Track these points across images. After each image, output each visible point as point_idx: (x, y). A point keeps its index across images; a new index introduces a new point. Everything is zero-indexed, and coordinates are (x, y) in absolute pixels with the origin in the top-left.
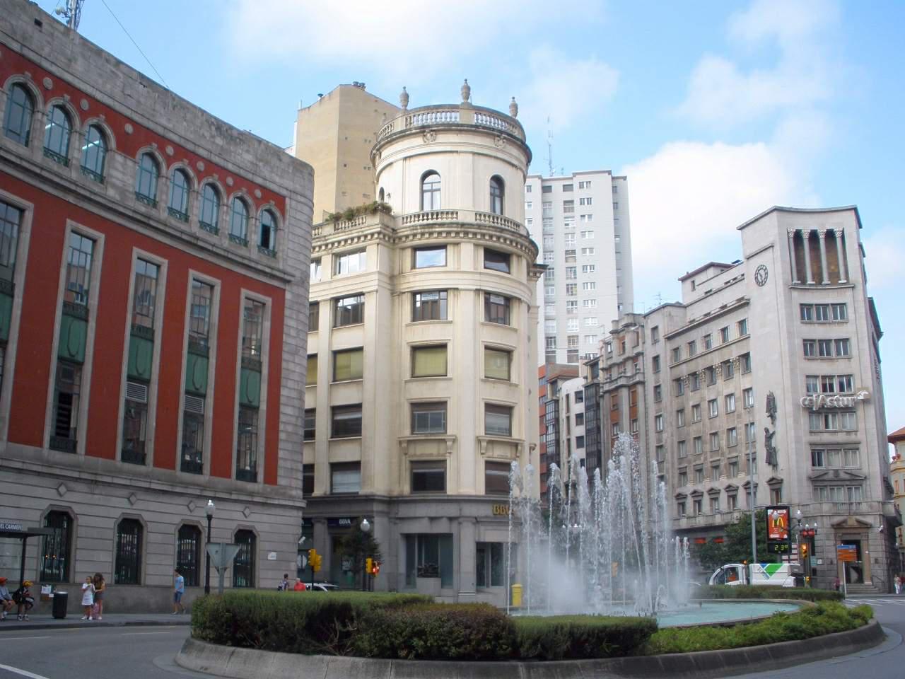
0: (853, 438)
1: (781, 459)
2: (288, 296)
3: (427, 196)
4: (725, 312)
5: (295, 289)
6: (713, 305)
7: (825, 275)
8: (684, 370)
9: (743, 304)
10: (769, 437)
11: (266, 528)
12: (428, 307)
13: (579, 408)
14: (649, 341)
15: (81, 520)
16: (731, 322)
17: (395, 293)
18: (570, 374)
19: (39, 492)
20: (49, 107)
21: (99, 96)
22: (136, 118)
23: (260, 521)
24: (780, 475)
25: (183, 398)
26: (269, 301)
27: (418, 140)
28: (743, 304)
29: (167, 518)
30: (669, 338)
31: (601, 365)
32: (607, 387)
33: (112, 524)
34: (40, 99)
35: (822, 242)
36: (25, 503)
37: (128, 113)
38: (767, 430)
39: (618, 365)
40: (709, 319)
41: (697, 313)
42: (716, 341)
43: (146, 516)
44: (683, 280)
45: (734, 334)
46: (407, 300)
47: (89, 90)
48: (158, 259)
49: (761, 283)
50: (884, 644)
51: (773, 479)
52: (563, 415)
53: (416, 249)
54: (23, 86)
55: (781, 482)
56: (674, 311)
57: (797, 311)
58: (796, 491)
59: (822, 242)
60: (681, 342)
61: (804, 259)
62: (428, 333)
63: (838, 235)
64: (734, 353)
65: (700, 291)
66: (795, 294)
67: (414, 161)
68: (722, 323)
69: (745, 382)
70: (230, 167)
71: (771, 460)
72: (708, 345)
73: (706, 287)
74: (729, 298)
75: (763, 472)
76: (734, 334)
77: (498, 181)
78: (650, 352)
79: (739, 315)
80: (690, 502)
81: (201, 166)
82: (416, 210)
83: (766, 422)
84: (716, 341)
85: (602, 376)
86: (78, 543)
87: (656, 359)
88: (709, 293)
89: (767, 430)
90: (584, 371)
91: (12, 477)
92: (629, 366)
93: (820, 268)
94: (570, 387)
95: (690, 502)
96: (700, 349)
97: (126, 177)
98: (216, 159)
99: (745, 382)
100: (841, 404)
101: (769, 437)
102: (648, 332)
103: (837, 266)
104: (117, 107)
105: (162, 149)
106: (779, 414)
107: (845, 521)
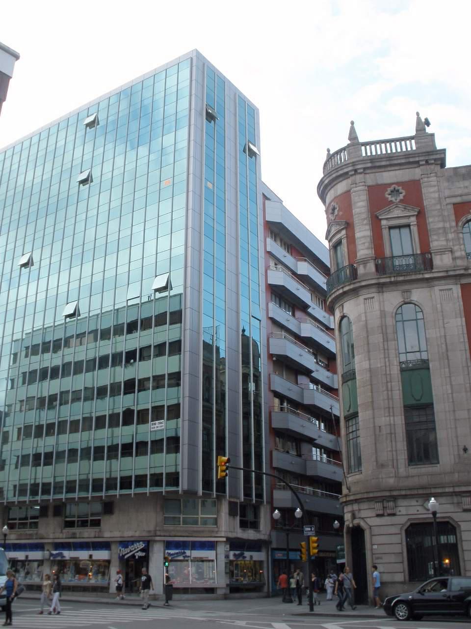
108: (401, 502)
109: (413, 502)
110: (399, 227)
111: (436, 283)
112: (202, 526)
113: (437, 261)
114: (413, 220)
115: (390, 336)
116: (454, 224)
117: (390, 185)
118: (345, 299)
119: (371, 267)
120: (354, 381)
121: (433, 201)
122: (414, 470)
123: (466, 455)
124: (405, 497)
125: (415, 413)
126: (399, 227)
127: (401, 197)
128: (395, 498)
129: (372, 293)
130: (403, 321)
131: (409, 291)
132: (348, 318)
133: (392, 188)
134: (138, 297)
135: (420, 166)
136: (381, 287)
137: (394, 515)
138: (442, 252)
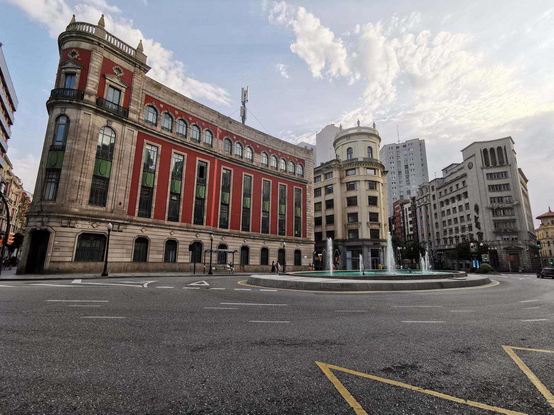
0: (513, 217)
1: (482, 226)
2: (307, 187)
3: (349, 155)
4: (458, 179)
5: (309, 185)
6: (454, 177)
7: (498, 162)
8: (443, 199)
9: (465, 175)
10: (476, 218)
11: (303, 249)
12: (351, 186)
13: (410, 212)
14: (431, 190)
15: (251, 249)
16: (460, 182)
17: (341, 183)
18: (407, 202)
19: (239, 242)
20: (235, 143)
21: (249, 139)
22: (260, 143)
23: (302, 247)
24: (482, 231)
25: (278, 215)
26: (302, 188)
27: (345, 139)
28: (465, 175)
29: (275, 247)
30: (438, 189)
31: (416, 199)
32: (418, 206)
33: (259, 249)
34: (233, 142)
35: (496, 152)
36: (235, 244)
37: (257, 142)
38: (475, 216)
39: (421, 199)
40: (452, 181)
41: (448, 180)
42: (454, 189)
43: (269, 247)
44: (443, 170)
45: (461, 186)
46: (345, 185)
47: (246, 137)
48: (269, 180)
49: (470, 168)
50: (515, 147)
51: (478, 233)
52: (405, 215)
53: (347, 171)
54: (228, 139)
55: (482, 233)
56: (439, 181)
57: (485, 176)
58: (488, 237)
59: (496, 152)
60: (442, 190)
61: (488, 160)
62: (352, 194)
63: (503, 148)
64: (461, 192)
65: (449, 173)
66: (484, 170)
67: (345, 145)
68: (457, 183)
69: (467, 201)
70: (288, 153)
71: (478, 225)
72: (451, 190)
73: (451, 172)
74: (459, 174)
75: (475, 230)
76: (461, 186)
77: (370, 148)
78: (432, 193)
79: (463, 180)
80: (448, 241)
81: (270, 151)
82: (346, 159)
83: (475, 214)
84: (454, 189)
85: (417, 202)
86: (250, 254)
87: (434, 196)
88: (452, 174)
89: (475, 216)
90: (411, 201)
91: (232, 238)
92: (425, 198)
93: (495, 160)
94: (407, 206)
95: (448, 241)
96: (448, 191)
97: (261, 160)
98: (283, 152)
99: (467, 201)
100: (506, 206)
101: (476, 218)
102: (431, 188)
103: (503, 158)
104: (254, 141)
105: (268, 151)
106: (480, 211)
107: (511, 247)
108: (79, 222)
109: (87, 223)
110: (115, 88)
111: (127, 125)
112: (436, 273)
113: (131, 115)
114: (124, 90)
115: (94, 138)
116: (143, 103)
117: (117, 65)
118: (69, 106)
119: (93, 99)
120: (60, 153)
121: (136, 87)
122: (90, 207)
123: (120, 206)
124: (83, 219)
125: (98, 180)
126: (115, 88)
127: (121, 75)
128: (77, 219)
129: (91, 112)
130: (104, 134)
131: (65, 109)
132: (68, 117)
133: (118, 67)
134: (244, 118)
135: (135, 66)
136: (97, 112)
137: (74, 227)
138: (135, 112)
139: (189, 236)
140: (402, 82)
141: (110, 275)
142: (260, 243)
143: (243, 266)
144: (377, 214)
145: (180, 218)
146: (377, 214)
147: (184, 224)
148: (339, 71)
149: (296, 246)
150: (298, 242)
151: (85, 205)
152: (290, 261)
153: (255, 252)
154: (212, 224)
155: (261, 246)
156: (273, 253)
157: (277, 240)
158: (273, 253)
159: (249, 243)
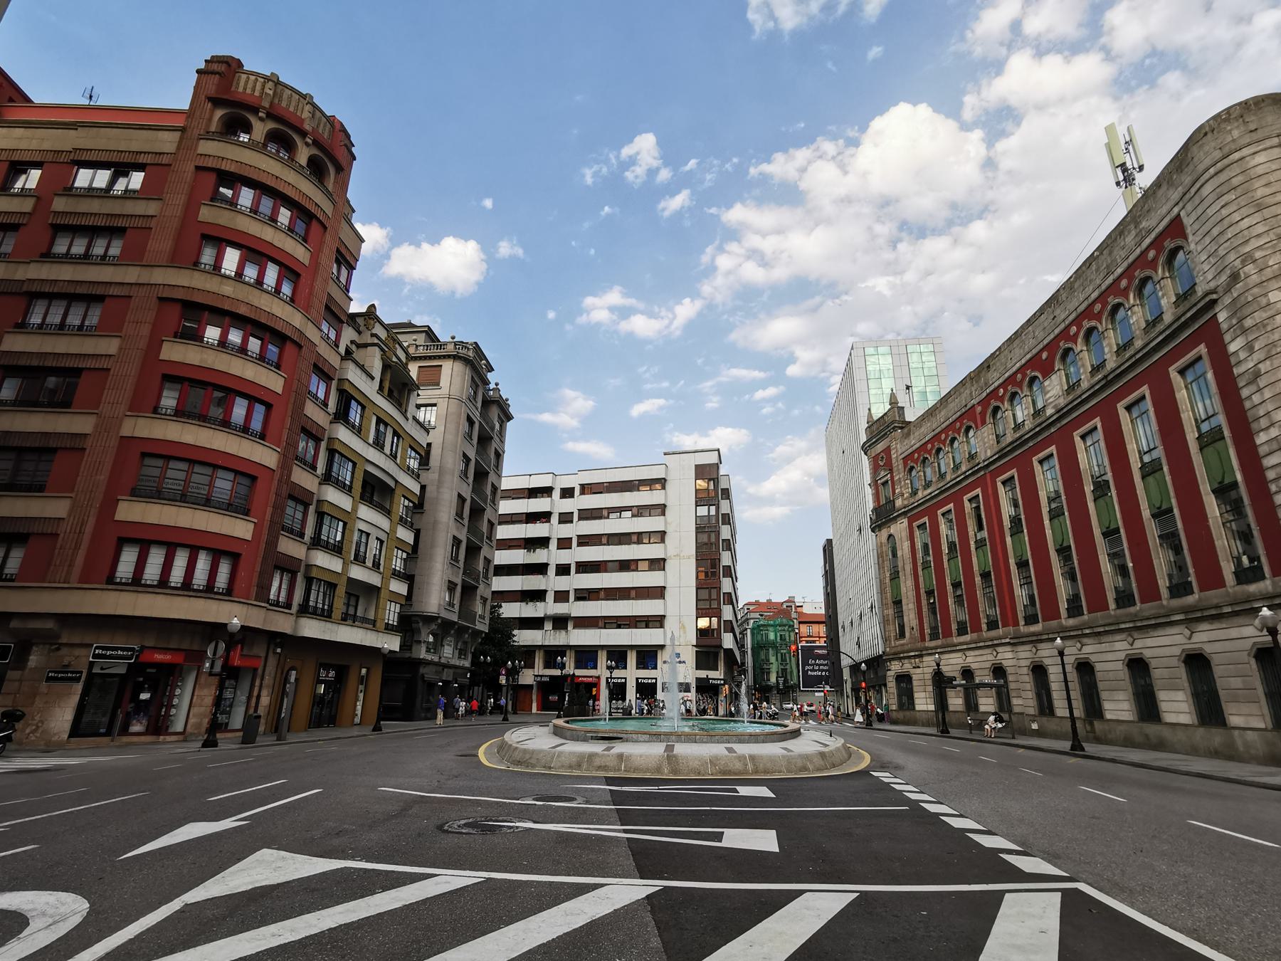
15: (1098, 667)
139: (984, 658)
140: (144, 696)
141: (953, 732)
142: (1119, 646)
143: (1091, 724)
144: (572, 496)
145: (1195, 585)
146: (572, 496)
147: (975, 635)
148: (664, 209)
149: (990, 657)
150: (1193, 618)
151: (1268, 582)
152: (1245, 708)
153: (1111, 676)
154: (1011, 621)
155: (1122, 655)
156: (1165, 673)
157: (1112, 630)
158: (1165, 673)
159: (1090, 649)
